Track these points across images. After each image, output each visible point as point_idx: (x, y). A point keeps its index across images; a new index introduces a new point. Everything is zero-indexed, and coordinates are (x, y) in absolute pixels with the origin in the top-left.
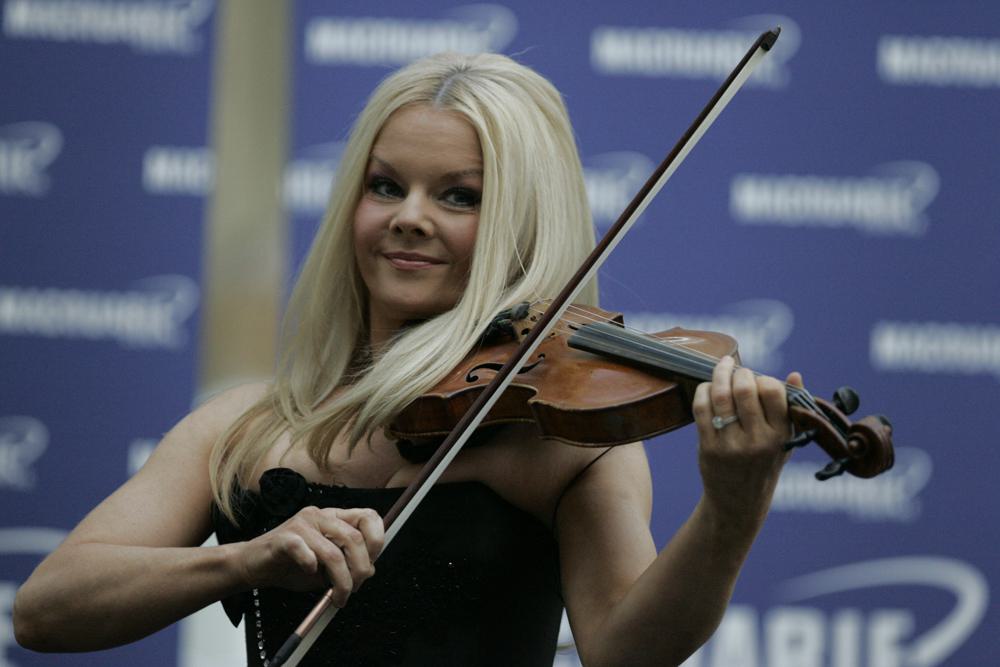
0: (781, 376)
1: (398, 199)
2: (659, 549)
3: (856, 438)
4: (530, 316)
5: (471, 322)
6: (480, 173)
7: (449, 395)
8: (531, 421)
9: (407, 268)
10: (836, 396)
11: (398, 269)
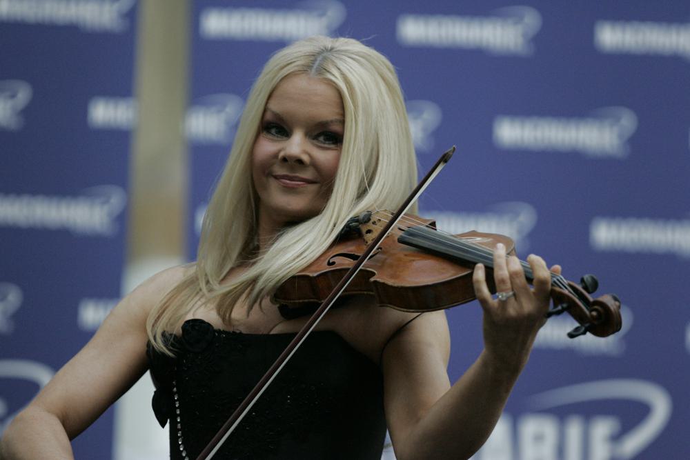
0: (523, 257)
1: (285, 138)
2: (452, 383)
3: (596, 310)
4: (372, 221)
5: (332, 224)
6: (343, 122)
7: (315, 275)
8: (371, 293)
9: (290, 186)
10: (582, 280)
11: (284, 187)
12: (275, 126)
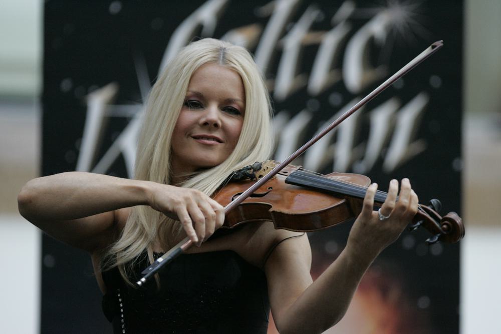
12: (195, 102)
